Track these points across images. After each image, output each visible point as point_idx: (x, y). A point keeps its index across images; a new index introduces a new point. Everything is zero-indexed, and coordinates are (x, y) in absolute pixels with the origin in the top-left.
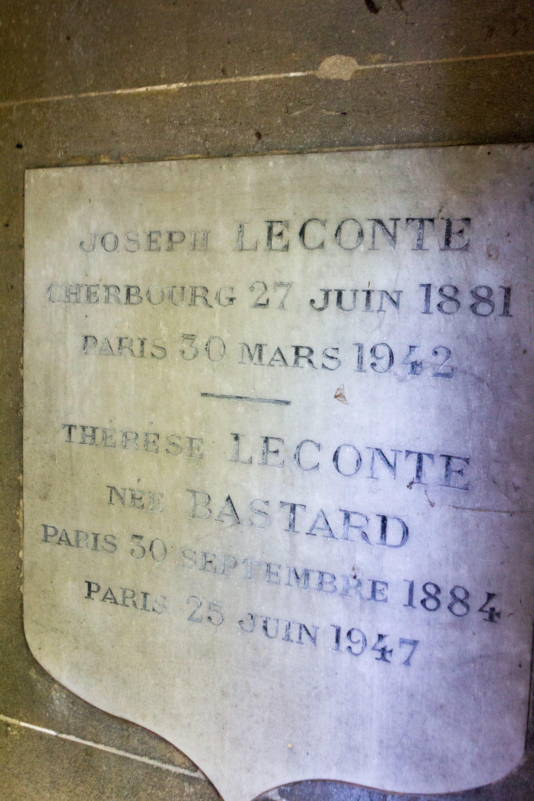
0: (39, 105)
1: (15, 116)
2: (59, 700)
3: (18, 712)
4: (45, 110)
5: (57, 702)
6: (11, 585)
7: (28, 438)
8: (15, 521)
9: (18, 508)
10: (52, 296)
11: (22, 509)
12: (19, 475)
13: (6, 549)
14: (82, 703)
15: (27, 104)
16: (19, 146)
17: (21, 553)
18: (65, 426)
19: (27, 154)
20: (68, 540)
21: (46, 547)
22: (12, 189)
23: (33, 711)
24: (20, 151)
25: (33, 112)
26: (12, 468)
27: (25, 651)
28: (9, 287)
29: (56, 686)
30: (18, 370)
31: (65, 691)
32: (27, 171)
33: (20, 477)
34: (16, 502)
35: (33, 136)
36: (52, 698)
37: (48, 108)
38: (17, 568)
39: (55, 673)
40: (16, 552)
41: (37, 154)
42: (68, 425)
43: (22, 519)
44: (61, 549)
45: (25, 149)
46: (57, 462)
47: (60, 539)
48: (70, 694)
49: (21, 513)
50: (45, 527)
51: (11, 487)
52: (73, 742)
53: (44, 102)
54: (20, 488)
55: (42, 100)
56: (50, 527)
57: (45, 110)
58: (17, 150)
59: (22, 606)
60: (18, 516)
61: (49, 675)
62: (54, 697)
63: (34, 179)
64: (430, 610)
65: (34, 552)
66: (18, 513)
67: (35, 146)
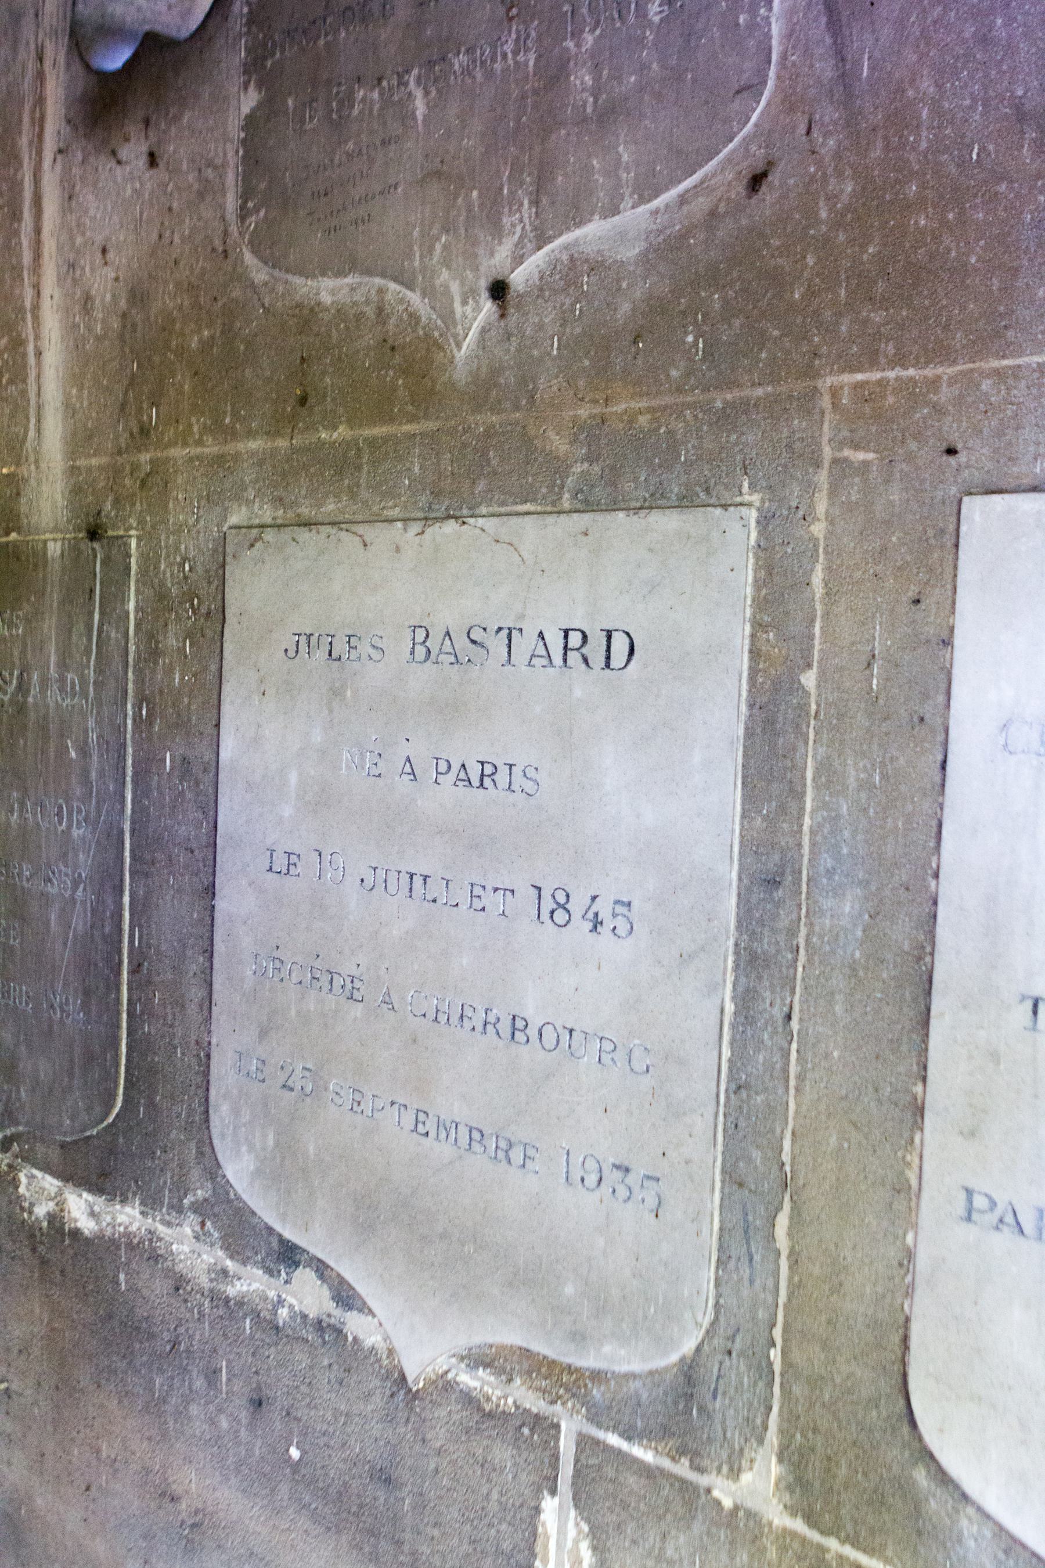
0: (999, 374)
1: (945, 394)
2: (976, 1540)
3: (883, 1546)
4: (1011, 381)
5: (972, 1543)
6: (884, 1296)
7: (942, 1014)
8: (902, 1173)
9: (909, 1148)
10: (1009, 742)
11: (918, 1151)
12: (915, 1084)
13: (878, 1225)
14: (1027, 1555)
15: (972, 370)
16: (951, 451)
17: (910, 1238)
18: (1023, 998)
19: (968, 467)
20: (1018, 1223)
21: (969, 1233)
22: (931, 533)
23: (915, 1552)
24: (952, 460)
25: (984, 387)
26: (901, 1069)
27: (906, 1429)
28: (916, 719)
29: (970, 1510)
30: (924, 880)
31: (991, 1524)
32: (966, 500)
33: (919, 1089)
34: (906, 1135)
35: (981, 432)
36: (960, 1534)
37: (1016, 378)
38: (901, 1265)
39: (971, 1485)
40: (901, 1232)
41: (989, 466)
42: (1029, 997)
43: (917, 1170)
44: (1006, 1238)
45: (962, 457)
46: (1002, 1067)
47: (1001, 1221)
48: (1000, 1530)
49: (917, 1161)
50: (969, 1192)
51: (896, 1104)
52: (130, 896)
53: (1010, 367)
54: (919, 1111)
55: (1005, 362)
56: (980, 1193)
57: (1011, 381)
58: (945, 457)
59: (905, 1339)
60: (909, 1164)
61: (957, 1487)
62: (966, 1532)
63: (978, 512)
64: (568, 922)
65: (939, 1237)
66: (908, 1158)
67: (984, 451)
